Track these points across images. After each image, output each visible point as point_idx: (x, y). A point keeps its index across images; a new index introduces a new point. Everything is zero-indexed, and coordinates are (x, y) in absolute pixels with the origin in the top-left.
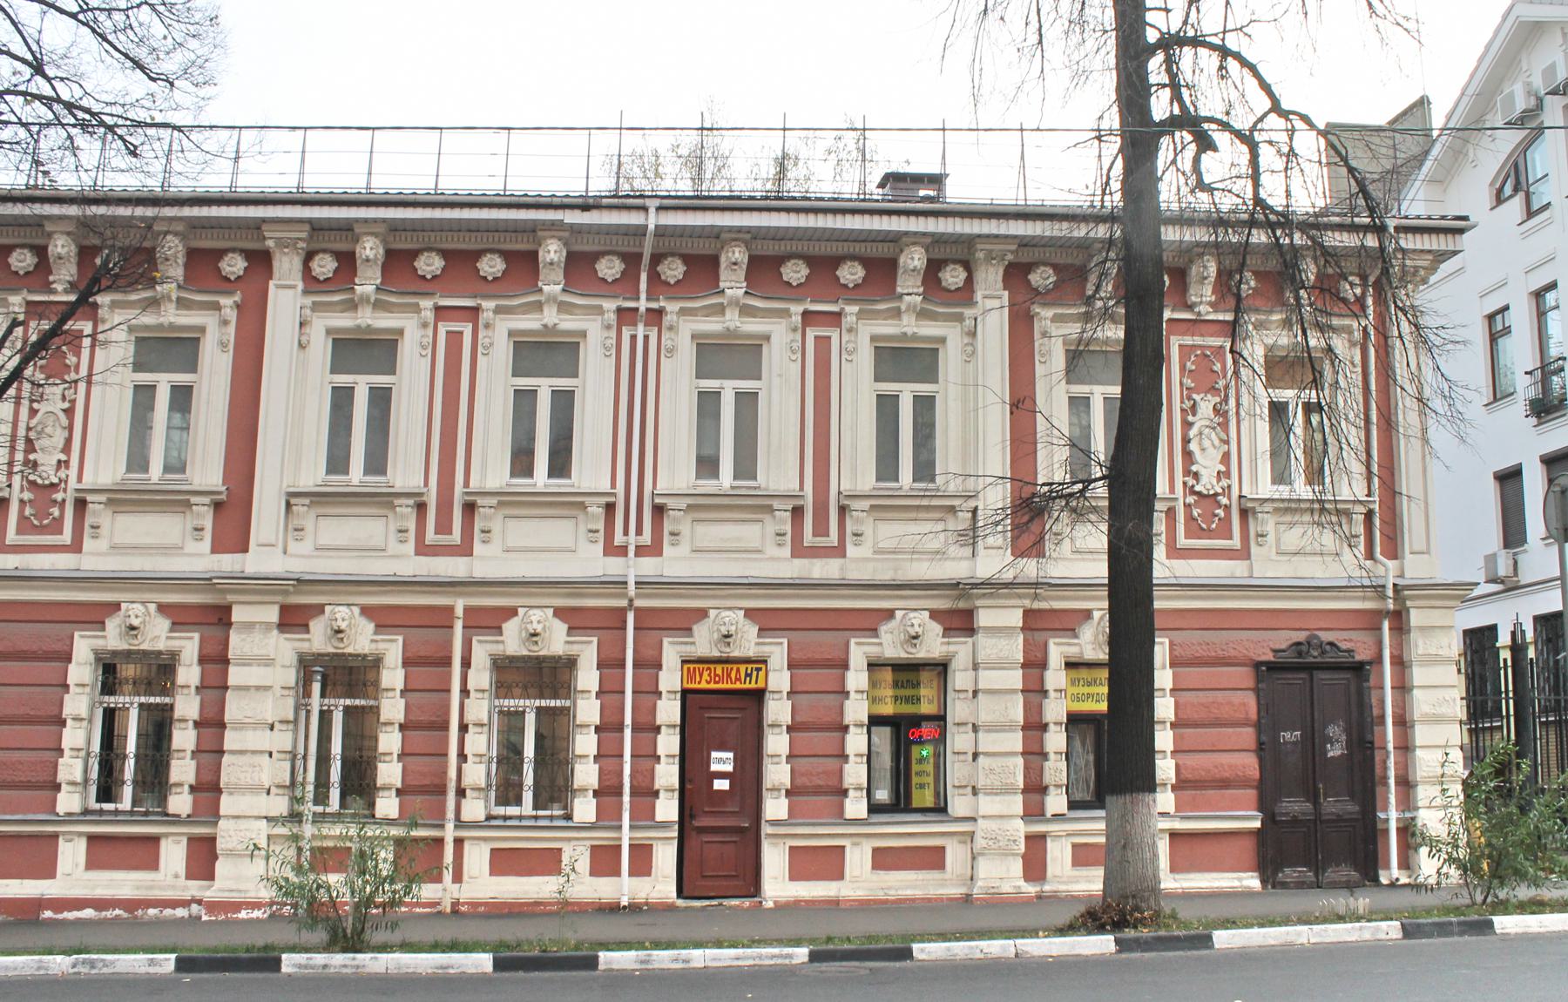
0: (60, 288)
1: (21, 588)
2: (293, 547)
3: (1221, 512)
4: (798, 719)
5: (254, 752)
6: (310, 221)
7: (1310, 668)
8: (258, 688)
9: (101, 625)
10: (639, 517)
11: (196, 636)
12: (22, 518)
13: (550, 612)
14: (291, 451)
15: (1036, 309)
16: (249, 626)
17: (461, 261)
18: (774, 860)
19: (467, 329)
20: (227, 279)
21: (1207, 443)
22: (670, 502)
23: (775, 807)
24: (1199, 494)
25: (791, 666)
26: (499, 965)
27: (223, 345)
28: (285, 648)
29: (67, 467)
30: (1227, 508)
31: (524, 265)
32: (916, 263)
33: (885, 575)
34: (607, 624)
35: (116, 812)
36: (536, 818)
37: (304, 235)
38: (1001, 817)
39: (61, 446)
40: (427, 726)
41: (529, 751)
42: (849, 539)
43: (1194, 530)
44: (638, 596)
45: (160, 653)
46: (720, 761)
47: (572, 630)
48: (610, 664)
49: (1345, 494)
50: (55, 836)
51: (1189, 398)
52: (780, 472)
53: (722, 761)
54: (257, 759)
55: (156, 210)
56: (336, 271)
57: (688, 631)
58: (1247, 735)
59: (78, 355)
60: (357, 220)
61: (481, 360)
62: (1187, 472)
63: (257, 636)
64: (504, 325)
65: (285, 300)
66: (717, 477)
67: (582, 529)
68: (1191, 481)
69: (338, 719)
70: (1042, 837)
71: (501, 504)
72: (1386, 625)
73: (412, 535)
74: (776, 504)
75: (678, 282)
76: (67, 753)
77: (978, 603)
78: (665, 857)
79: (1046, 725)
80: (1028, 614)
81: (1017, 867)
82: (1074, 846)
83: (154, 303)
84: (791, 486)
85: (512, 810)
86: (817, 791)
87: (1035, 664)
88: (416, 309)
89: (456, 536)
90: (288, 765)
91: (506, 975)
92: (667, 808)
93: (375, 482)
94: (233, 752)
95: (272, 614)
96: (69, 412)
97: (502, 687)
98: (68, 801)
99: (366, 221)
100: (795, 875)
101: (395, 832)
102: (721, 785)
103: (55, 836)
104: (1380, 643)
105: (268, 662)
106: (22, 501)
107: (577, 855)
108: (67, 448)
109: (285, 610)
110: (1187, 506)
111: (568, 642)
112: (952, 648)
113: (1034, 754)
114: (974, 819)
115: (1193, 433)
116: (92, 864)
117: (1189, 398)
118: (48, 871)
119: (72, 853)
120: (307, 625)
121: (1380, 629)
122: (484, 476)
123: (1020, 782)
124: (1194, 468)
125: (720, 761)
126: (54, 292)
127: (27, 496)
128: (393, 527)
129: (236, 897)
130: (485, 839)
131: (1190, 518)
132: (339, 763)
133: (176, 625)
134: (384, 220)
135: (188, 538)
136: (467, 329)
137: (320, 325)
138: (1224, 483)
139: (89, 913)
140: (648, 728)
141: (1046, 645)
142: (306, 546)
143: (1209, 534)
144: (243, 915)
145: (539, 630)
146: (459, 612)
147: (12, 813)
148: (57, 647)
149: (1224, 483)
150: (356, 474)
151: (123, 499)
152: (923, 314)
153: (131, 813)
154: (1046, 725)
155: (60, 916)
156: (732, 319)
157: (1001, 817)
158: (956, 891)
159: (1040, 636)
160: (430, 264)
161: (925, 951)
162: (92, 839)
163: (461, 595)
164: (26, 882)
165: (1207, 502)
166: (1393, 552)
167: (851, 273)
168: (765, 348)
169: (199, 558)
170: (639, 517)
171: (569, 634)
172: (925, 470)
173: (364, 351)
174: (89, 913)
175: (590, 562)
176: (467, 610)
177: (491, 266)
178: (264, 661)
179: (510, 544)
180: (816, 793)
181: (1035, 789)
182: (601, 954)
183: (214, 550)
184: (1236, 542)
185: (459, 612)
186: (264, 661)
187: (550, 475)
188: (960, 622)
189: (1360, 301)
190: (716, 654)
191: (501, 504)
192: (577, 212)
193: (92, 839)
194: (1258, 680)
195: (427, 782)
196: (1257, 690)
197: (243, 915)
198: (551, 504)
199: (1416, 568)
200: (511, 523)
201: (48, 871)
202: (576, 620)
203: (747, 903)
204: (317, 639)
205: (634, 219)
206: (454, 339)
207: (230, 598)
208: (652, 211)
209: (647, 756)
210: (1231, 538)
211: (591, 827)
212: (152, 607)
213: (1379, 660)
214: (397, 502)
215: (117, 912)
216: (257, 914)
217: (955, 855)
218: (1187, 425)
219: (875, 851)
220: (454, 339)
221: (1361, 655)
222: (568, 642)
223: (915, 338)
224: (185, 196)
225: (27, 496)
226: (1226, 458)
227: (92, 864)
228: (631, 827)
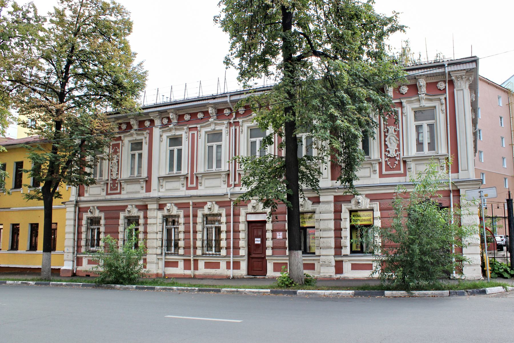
2: (161, 190)
3: (397, 162)
4: (274, 228)
6: (158, 111)
9: (350, 201)
10: (193, 179)
11: (378, 203)
14: (161, 167)
16: (151, 209)
17: (193, 115)
18: (270, 267)
19: (196, 133)
20: (402, 94)
21: (392, 141)
23: (269, 252)
24: (390, 157)
25: (380, 210)
27: (146, 143)
28: (160, 214)
30: (399, 161)
36: (216, 254)
38: (328, 255)
43: (388, 168)
46: (257, 241)
47: (220, 207)
48: (187, 216)
51: (386, 128)
53: (258, 241)
54: (153, 241)
56: (191, 118)
60: (167, 109)
62: (386, 151)
63: (152, 212)
64: (203, 130)
65: (156, 131)
66: (423, 151)
68: (387, 153)
72: (452, 195)
76: (343, 238)
78: (244, 265)
80: (335, 197)
81: (333, 270)
83: (209, 125)
85: (211, 253)
86: (279, 248)
87: (338, 212)
89: (194, 185)
90: (160, 242)
92: (243, 252)
93: (432, 153)
96: (118, 162)
99: (169, 109)
100: (275, 270)
107: (223, 265)
108: (118, 171)
109: (160, 205)
110: (386, 161)
112: (314, 208)
113: (338, 237)
114: (320, 256)
117: (386, 128)
121: (450, 196)
122: (411, 153)
123: (333, 245)
124: (387, 149)
125: (257, 241)
127: (111, 182)
130: (203, 260)
131: (387, 165)
133: (220, 207)
135: (372, 173)
136: (196, 133)
137: (165, 136)
140: (236, 231)
143: (393, 169)
146: (191, 204)
149: (398, 153)
150: (426, 152)
151: (129, 181)
157: (326, 255)
159: (339, 203)
160: (187, 117)
165: (393, 159)
166: (456, 170)
169: (143, 194)
173: (175, 141)
175: (183, 192)
176: (193, 203)
177: (200, 116)
178: (155, 218)
180: (280, 248)
181: (338, 247)
183: (146, 192)
184: (402, 171)
185: (191, 204)
186: (155, 218)
187: (429, 150)
189: (445, 89)
190: (253, 211)
199: (462, 175)
200: (206, 181)
203: (263, 277)
204: (166, 213)
206: (193, 135)
207: (147, 203)
209: (236, 239)
211: (225, 257)
212: (214, 203)
218: (386, 136)
219: (352, 264)
220: (193, 135)
226: (399, 146)
228: (233, 257)
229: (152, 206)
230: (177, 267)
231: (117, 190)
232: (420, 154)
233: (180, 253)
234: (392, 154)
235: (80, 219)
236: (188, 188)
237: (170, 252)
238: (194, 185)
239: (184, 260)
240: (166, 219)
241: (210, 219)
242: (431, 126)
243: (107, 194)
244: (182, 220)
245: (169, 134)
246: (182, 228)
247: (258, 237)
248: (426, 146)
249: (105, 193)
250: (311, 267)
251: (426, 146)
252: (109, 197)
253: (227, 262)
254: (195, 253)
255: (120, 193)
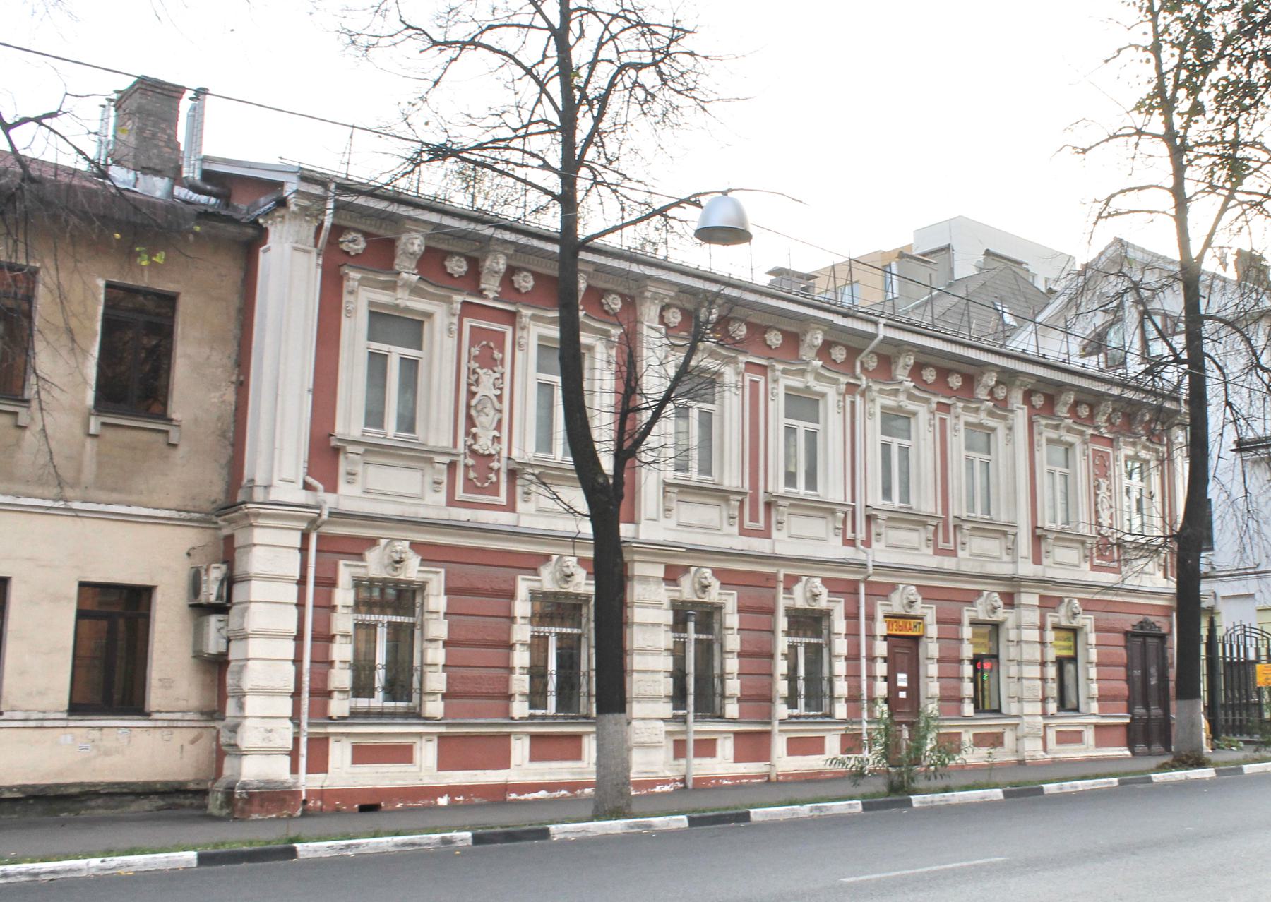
0: (491, 295)
1: (478, 537)
5: (653, 671)
7: (1145, 636)
8: (653, 624)
10: (759, 509)
11: (442, 571)
12: (467, 480)
13: (407, 544)
15: (346, 270)
19: (761, 380)
22: (880, 515)
25: (448, 591)
26: (692, 822)
28: (663, 594)
29: (499, 442)
31: (793, 341)
32: (416, 248)
33: (977, 570)
34: (846, 589)
35: (544, 717)
37: (672, 294)
39: (494, 425)
40: (758, 655)
41: (552, 665)
42: (873, 537)
44: (874, 574)
45: (579, 595)
47: (424, 561)
48: (852, 616)
49: (432, 442)
50: (508, 735)
52: (437, 429)
55: (1107, 387)
57: (360, 556)
58: (1121, 671)
59: (502, 351)
61: (771, 404)
62: (468, 433)
63: (653, 587)
64: (785, 381)
67: (725, 514)
68: (470, 441)
69: (801, 650)
70: (325, 739)
71: (791, 505)
73: (444, 486)
74: (438, 458)
75: (527, 292)
77: (636, 557)
79: (513, 645)
82: (1058, 732)
84: (445, 444)
88: (449, 301)
89: (761, 524)
91: (872, 813)
94: (638, 671)
95: (660, 572)
97: (539, 618)
98: (520, 708)
101: (1094, 720)
102: (902, 695)
103: (508, 735)
104: (858, 602)
105: (657, 605)
106: (466, 466)
108: (499, 427)
109: (669, 568)
111: (420, 571)
115: (473, 402)
116: (533, 758)
118: (504, 763)
119: (520, 749)
120: (535, 569)
124: (474, 430)
126: (486, 297)
127: (470, 462)
128: (428, 479)
129: (651, 777)
132: (554, 677)
134: (594, 263)
138: (497, 447)
139: (542, 794)
141: (514, 580)
142: (672, 523)
144: (658, 789)
145: (807, 593)
146: (781, 577)
147: (485, 717)
148: (505, 586)
152: (415, 291)
153: (553, 717)
154: (513, 645)
155: (522, 797)
156: (811, 381)
158: (1013, 759)
161: (1050, 788)
162: (534, 737)
163: (784, 566)
164: (487, 772)
167: (955, 381)
168: (426, 326)
170: (480, 473)
171: (421, 565)
172: (407, 423)
174: (542, 794)
179: (793, 533)
182: (752, 811)
184: (502, 498)
185: (781, 577)
188: (1009, 601)
191: (791, 505)
192: (840, 317)
193: (534, 737)
194: (1127, 640)
195: (753, 693)
196: (1126, 647)
197: (658, 789)
198: (814, 508)
201: (504, 763)
202: (834, 587)
204: (686, 590)
205: (869, 328)
206: (754, 384)
208: (881, 326)
210: (497, 494)
213: (1170, 633)
214: (732, 497)
215: (563, 792)
216: (667, 788)
217: (1009, 737)
220: (754, 384)
221: (1164, 631)
222: (420, 571)
223: (407, 309)
224: (542, 232)
225: (470, 462)
227: (533, 758)
229: (1029, 598)
230: (326, 771)
231: (496, 493)
232: (374, 436)
233: (728, 715)
234: (484, 444)
235: (327, 583)
236: (744, 532)
237: (539, 712)
238: (951, 546)
239: (1097, 726)
240: (681, 614)
241: (809, 622)
242: (410, 366)
243: (452, 502)
244: (840, 624)
245: (383, 297)
246: (841, 646)
247: (902, 672)
248: (694, 465)
249: (442, 497)
250: (996, 740)
251: (694, 465)
252: (462, 515)
253: (676, 742)
254: (871, 711)
255: (511, 507)
